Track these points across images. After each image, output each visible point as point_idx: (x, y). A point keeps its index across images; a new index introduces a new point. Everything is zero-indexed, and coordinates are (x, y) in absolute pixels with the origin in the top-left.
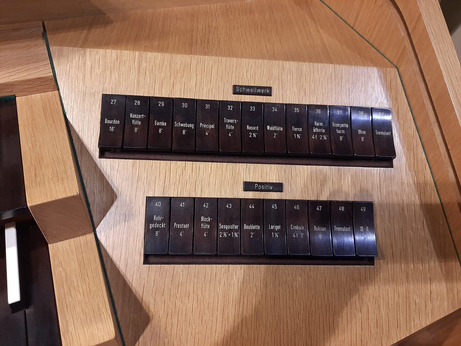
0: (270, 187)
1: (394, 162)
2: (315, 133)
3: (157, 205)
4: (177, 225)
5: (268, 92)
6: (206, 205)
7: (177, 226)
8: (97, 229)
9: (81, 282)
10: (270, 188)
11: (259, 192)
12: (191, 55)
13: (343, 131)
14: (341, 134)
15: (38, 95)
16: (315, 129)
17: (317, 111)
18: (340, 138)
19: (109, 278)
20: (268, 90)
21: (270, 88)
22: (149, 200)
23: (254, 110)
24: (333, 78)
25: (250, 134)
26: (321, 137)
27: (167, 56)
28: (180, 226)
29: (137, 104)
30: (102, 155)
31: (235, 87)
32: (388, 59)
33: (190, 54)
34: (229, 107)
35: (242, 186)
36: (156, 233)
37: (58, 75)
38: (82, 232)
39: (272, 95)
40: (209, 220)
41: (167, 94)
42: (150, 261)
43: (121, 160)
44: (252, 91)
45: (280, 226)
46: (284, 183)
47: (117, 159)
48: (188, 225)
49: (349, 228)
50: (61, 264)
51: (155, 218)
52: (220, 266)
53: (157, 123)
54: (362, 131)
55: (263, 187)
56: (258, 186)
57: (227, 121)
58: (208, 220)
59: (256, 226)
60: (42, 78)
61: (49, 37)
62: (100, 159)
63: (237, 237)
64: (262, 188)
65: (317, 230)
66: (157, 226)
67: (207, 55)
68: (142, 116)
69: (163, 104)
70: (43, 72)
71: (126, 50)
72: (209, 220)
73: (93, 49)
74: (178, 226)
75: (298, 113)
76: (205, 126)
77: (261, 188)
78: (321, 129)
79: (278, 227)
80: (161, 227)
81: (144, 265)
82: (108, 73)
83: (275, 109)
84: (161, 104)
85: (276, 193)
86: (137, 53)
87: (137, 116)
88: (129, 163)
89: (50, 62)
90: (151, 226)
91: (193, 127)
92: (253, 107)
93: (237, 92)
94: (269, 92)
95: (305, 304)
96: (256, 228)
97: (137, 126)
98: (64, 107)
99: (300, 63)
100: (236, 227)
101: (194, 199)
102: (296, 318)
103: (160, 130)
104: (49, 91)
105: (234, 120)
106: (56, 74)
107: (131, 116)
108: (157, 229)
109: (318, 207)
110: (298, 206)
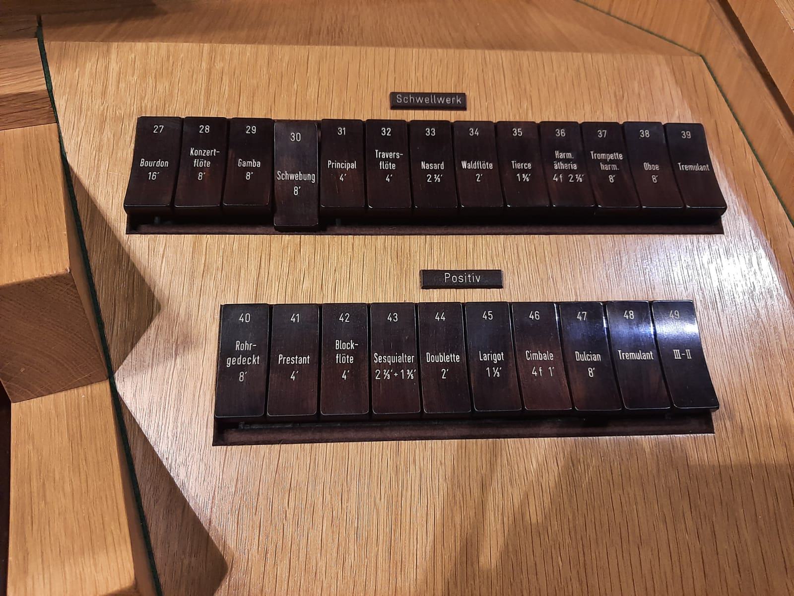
0: (475, 277)
1: (723, 222)
2: (559, 172)
3: (243, 320)
4: (284, 358)
5: (459, 102)
6: (345, 318)
7: (286, 360)
8: (116, 375)
9: (69, 471)
10: (475, 279)
11: (455, 290)
12: (307, 46)
13: (614, 165)
14: (611, 172)
15: (19, 130)
16: (557, 163)
17: (558, 132)
18: (609, 179)
19: (138, 476)
20: (458, 99)
21: (463, 96)
22: (227, 311)
23: (395, 319)
24: (583, 75)
25: (429, 176)
26: (571, 178)
27: (264, 49)
28: (291, 361)
29: (204, 132)
30: (134, 227)
31: (393, 95)
32: (682, 46)
33: (305, 45)
34: (384, 131)
35: (417, 279)
36: (241, 376)
37: (57, 89)
38: (83, 377)
39: (468, 108)
40: (352, 346)
41: (263, 114)
42: (230, 439)
43: (170, 235)
44: (427, 101)
45: (502, 354)
46: (503, 270)
47: (163, 235)
48: (308, 358)
49: (650, 353)
50: (33, 438)
51: (237, 346)
52: (380, 445)
53: (242, 163)
54: (651, 165)
55: (461, 278)
56: (451, 277)
57: (381, 155)
58: (349, 346)
59: (451, 356)
60: (25, 95)
61: (45, 32)
62: (127, 235)
63: (412, 378)
64: (462, 277)
65: (583, 360)
66: (243, 361)
67: (339, 44)
68: (213, 152)
69: (255, 130)
70: (27, 84)
71: (186, 42)
72: (352, 346)
73: (125, 43)
74: (287, 360)
75: (520, 136)
76: (339, 165)
77: (457, 281)
78: (570, 163)
79: (498, 357)
80: (252, 363)
81: (215, 447)
82: (151, 81)
83: (474, 132)
84: (250, 131)
85: (488, 290)
86: (207, 46)
87: (203, 152)
88: (186, 241)
89: (42, 67)
90: (230, 362)
91: (314, 180)
92: (432, 130)
93: (399, 105)
94: (460, 102)
95: (571, 525)
96: (453, 360)
97: (202, 169)
98: (63, 144)
99: (516, 52)
100: (410, 359)
101: (320, 306)
102: (554, 556)
103: (248, 174)
104: (40, 122)
105: (394, 153)
106: (52, 88)
107: (192, 152)
108: (242, 368)
109: (579, 313)
110: (537, 313)
